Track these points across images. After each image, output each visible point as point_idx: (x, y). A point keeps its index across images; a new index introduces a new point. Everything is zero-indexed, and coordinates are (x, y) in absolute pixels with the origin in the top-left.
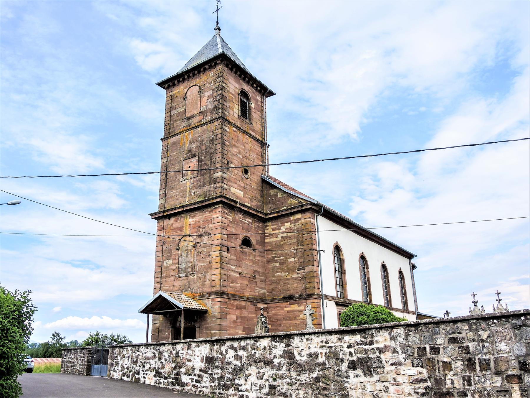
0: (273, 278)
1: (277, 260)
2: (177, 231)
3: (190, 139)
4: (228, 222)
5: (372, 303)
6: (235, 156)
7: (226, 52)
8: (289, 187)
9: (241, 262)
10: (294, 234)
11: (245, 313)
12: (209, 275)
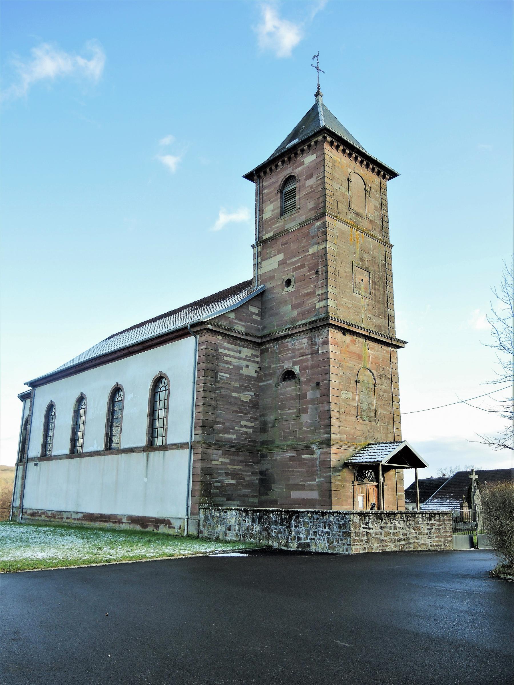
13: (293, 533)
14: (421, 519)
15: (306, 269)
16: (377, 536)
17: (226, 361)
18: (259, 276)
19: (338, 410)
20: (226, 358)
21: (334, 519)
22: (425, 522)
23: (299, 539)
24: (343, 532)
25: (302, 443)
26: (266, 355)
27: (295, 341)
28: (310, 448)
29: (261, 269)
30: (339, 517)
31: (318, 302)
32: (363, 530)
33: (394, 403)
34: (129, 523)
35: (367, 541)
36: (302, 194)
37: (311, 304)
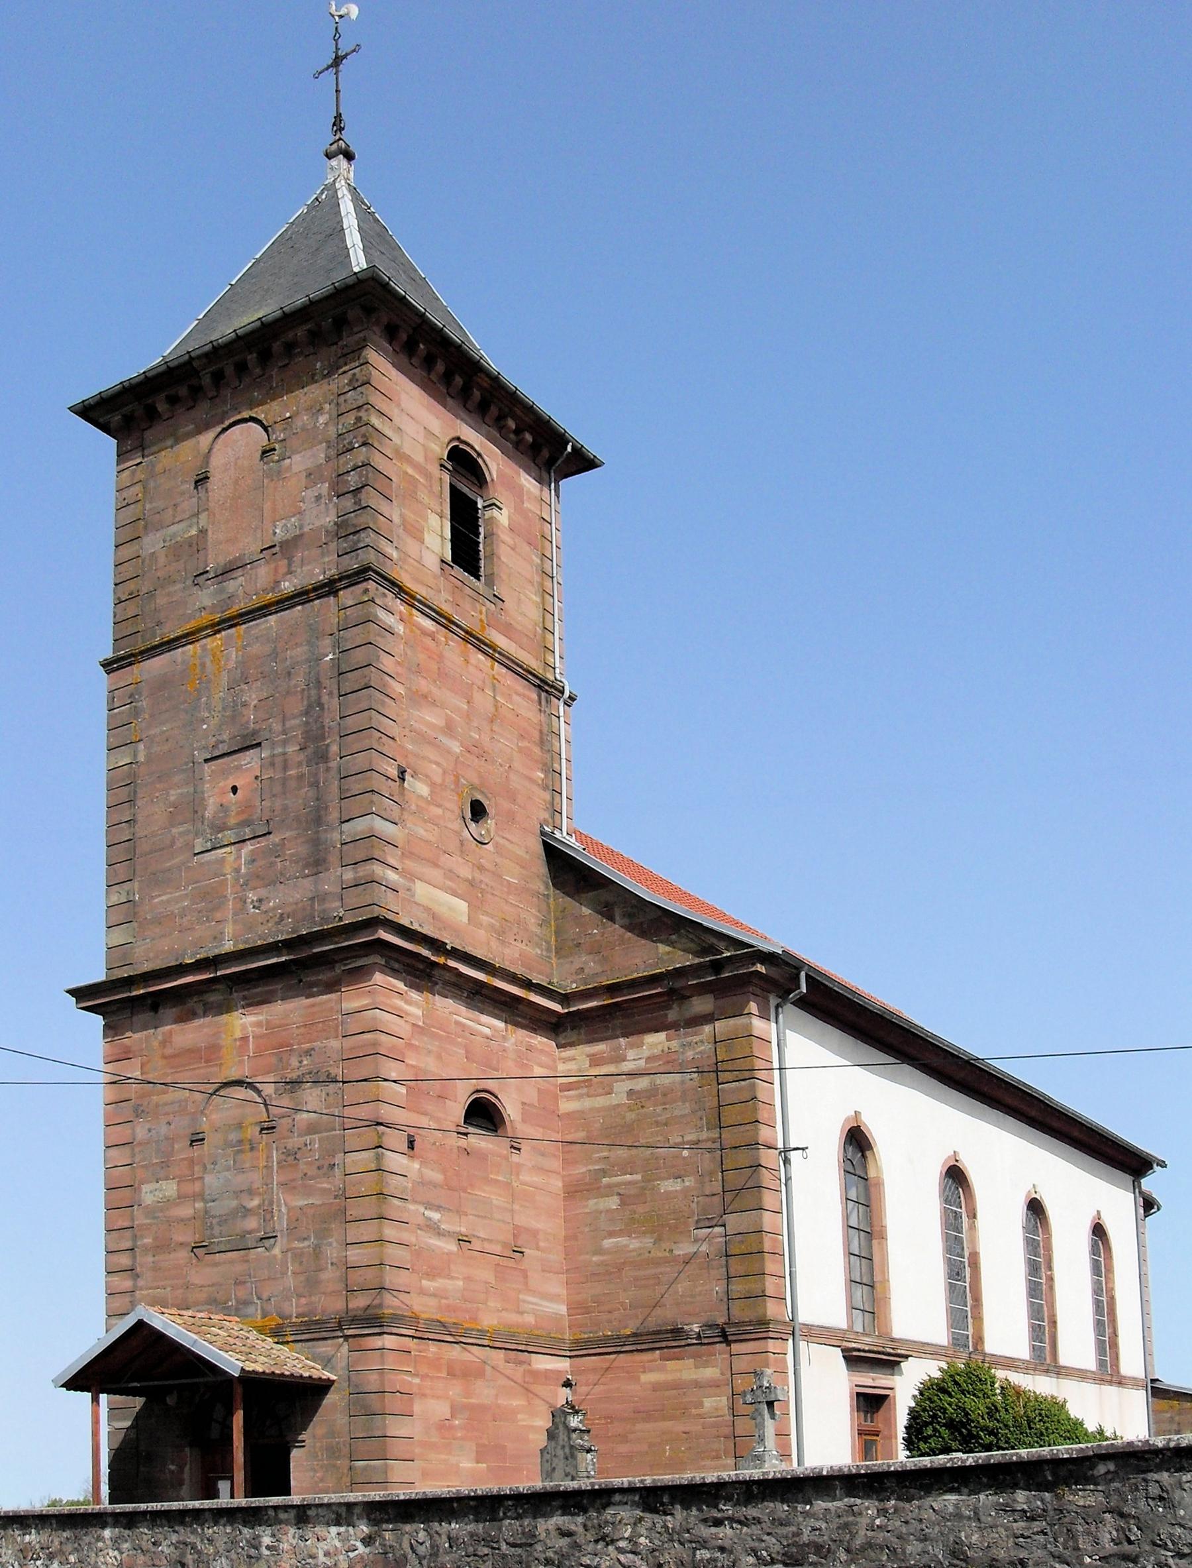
0: (595, 1259)
1: (609, 1186)
2: (189, 1064)
3: (232, 664)
4: (408, 1027)
5: (983, 1350)
6: (429, 743)
7: (387, 271)
8: (697, 900)
9: (462, 1194)
10: (683, 1082)
11: (484, 1393)
12: (335, 1244)
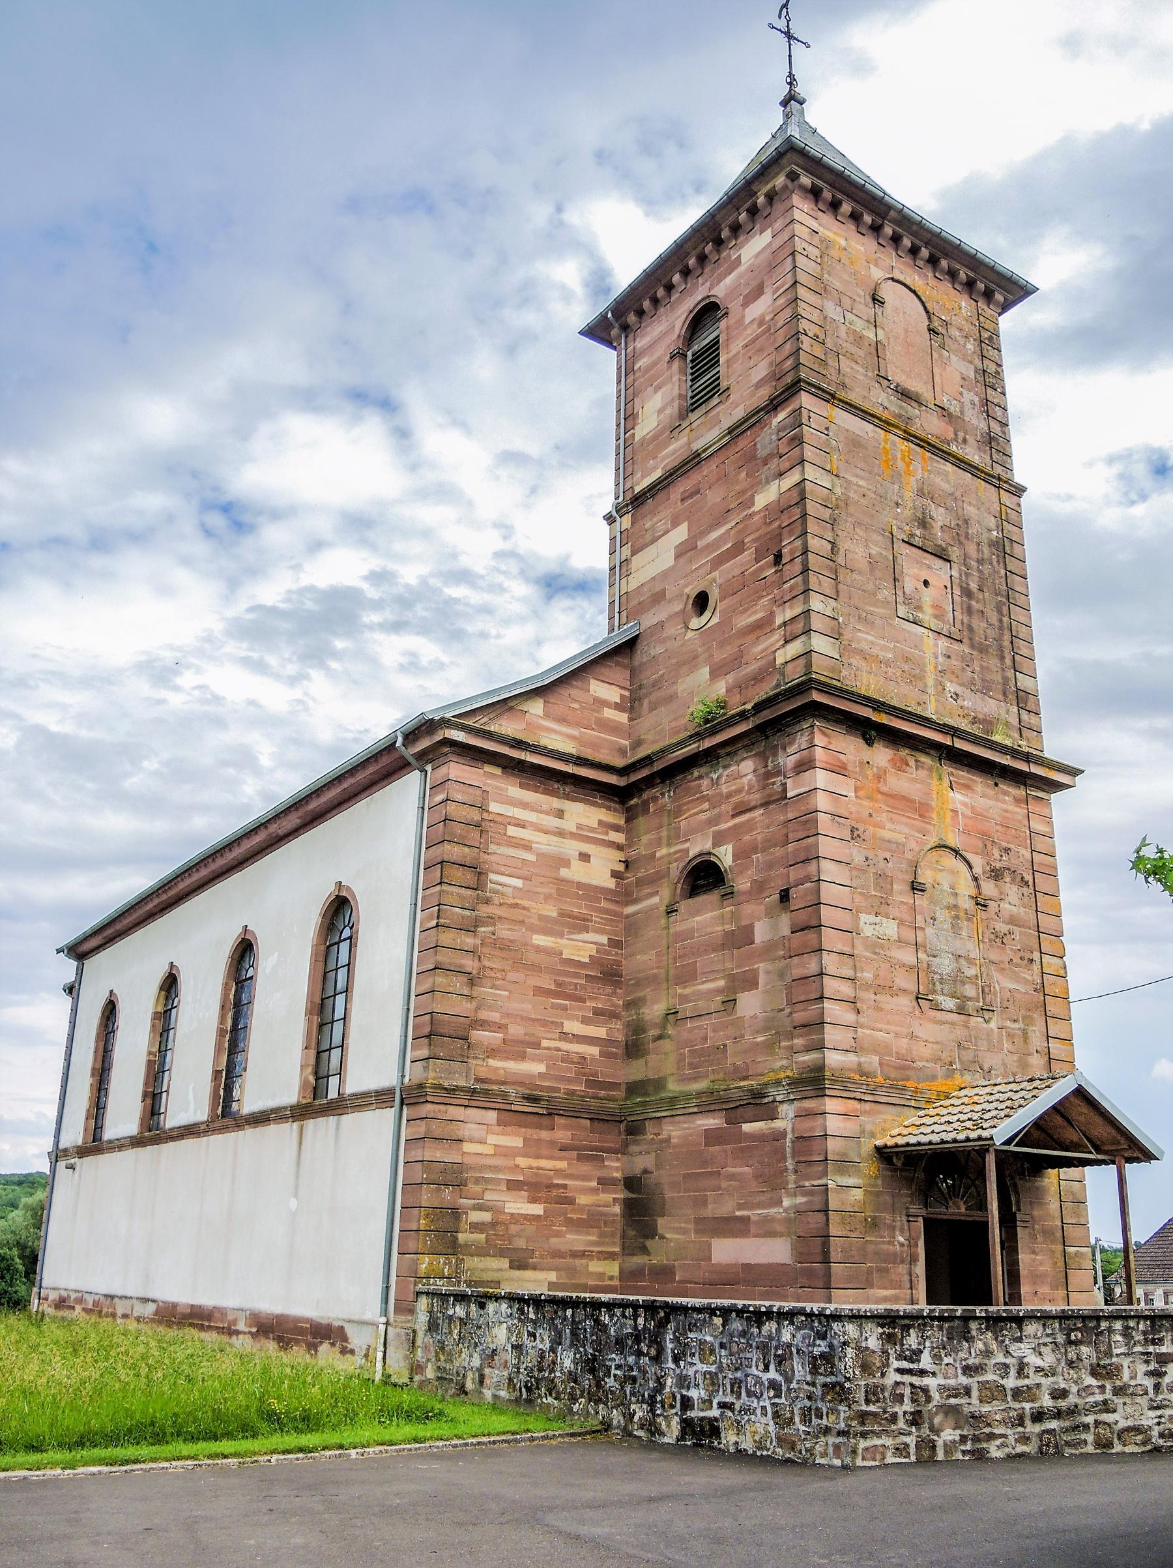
2: (903, 810)
13: (669, 1382)
14: (1119, 1338)
15: (748, 555)
16: (952, 1401)
17: (514, 840)
18: (624, 598)
19: (850, 973)
20: (512, 831)
21: (794, 1336)
22: (1136, 1349)
23: (687, 1403)
24: (825, 1385)
25: (742, 1084)
26: (641, 821)
27: (721, 770)
28: (766, 1100)
29: (630, 578)
30: (812, 1328)
31: (783, 646)
32: (898, 1378)
33: (1046, 958)
34: (250, 1333)
35: (916, 1419)
36: (736, 346)
37: (764, 654)
